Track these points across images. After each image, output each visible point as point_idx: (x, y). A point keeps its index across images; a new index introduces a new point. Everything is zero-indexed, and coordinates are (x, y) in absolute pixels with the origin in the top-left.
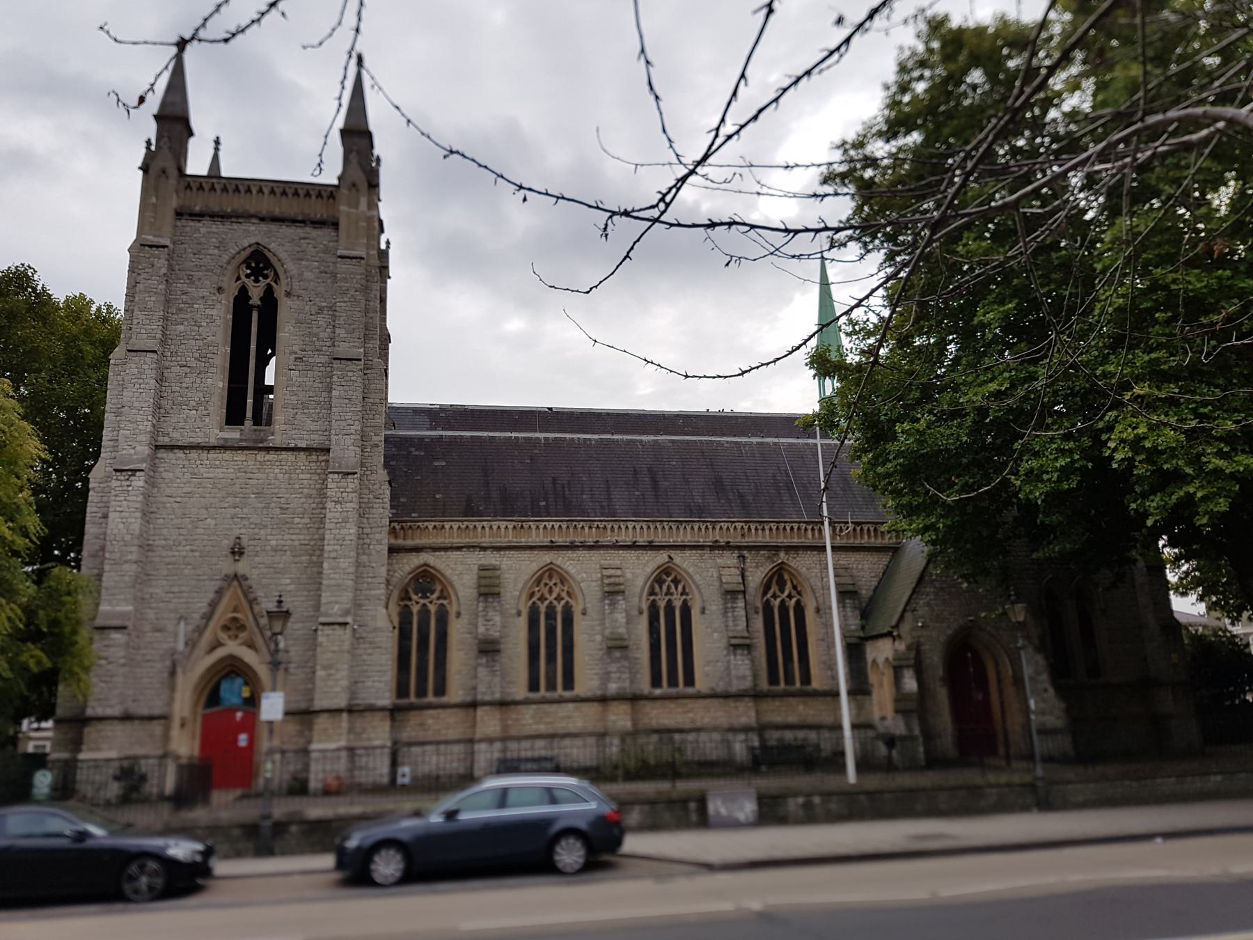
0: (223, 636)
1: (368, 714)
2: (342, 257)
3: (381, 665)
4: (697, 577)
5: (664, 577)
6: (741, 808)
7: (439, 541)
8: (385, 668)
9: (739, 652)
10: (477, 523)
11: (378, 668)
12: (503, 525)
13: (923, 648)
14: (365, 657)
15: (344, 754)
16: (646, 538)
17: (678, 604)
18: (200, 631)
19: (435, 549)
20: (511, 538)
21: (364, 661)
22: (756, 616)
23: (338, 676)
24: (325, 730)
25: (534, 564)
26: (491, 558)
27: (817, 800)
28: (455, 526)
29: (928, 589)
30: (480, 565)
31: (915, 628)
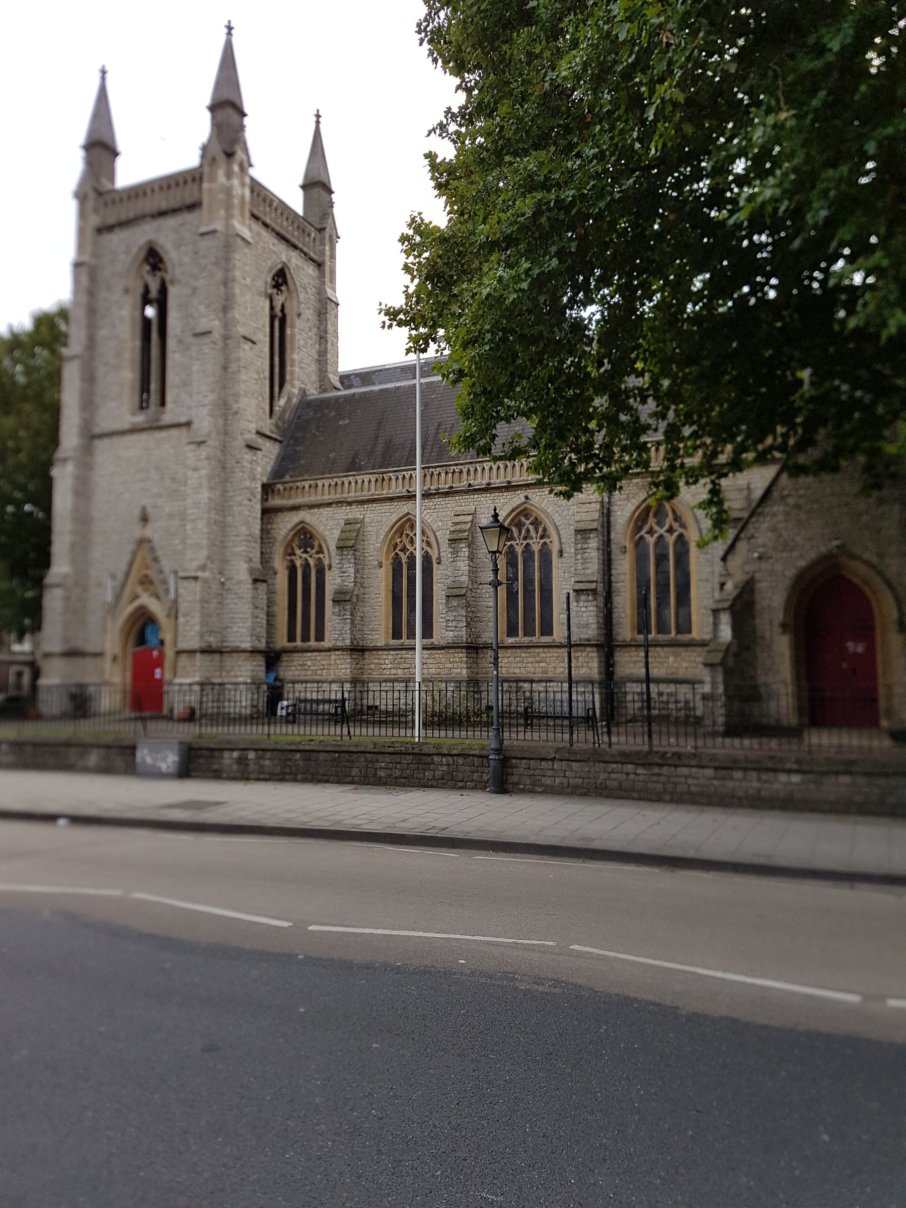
0: (139, 589)
1: (234, 655)
2: (202, 235)
3: (244, 613)
4: (556, 517)
5: (523, 519)
6: (164, 759)
7: (313, 499)
8: (246, 616)
9: (583, 598)
10: (344, 479)
11: (242, 616)
12: (366, 478)
13: (758, 586)
14: (232, 606)
15: (197, 688)
16: (502, 479)
17: (536, 548)
18: (123, 586)
19: (311, 507)
20: (374, 491)
21: (231, 609)
22: (622, 557)
23: (193, 622)
24: (185, 667)
25: (394, 515)
26: (355, 513)
27: (251, 755)
28: (327, 483)
29: (775, 509)
30: (347, 520)
31: (747, 562)
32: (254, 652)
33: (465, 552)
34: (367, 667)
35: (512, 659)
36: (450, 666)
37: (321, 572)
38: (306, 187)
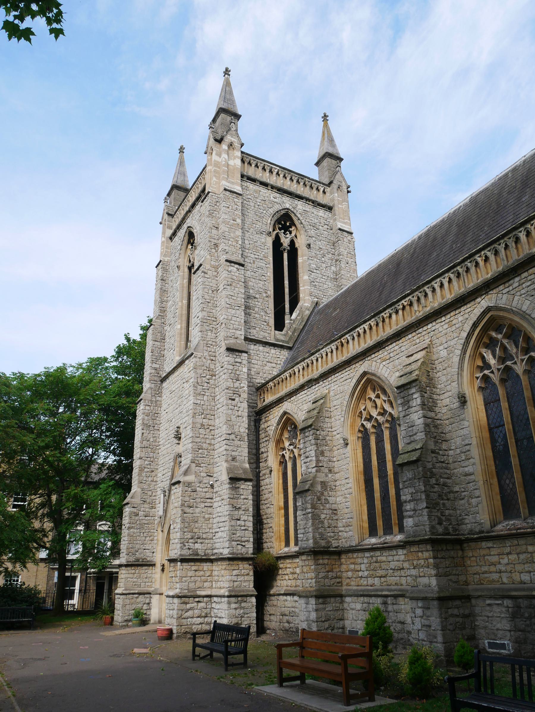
32: (233, 559)
33: (417, 400)
34: (344, 574)
35: (513, 557)
36: (414, 572)
37: (294, 460)
38: (30, 39)
